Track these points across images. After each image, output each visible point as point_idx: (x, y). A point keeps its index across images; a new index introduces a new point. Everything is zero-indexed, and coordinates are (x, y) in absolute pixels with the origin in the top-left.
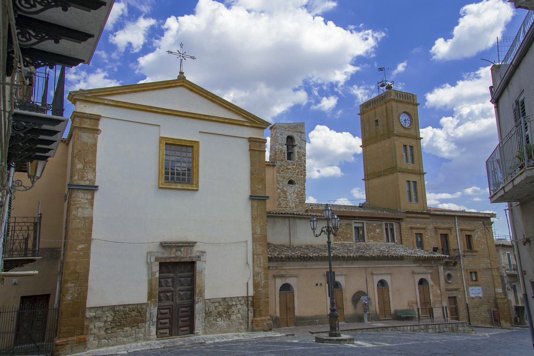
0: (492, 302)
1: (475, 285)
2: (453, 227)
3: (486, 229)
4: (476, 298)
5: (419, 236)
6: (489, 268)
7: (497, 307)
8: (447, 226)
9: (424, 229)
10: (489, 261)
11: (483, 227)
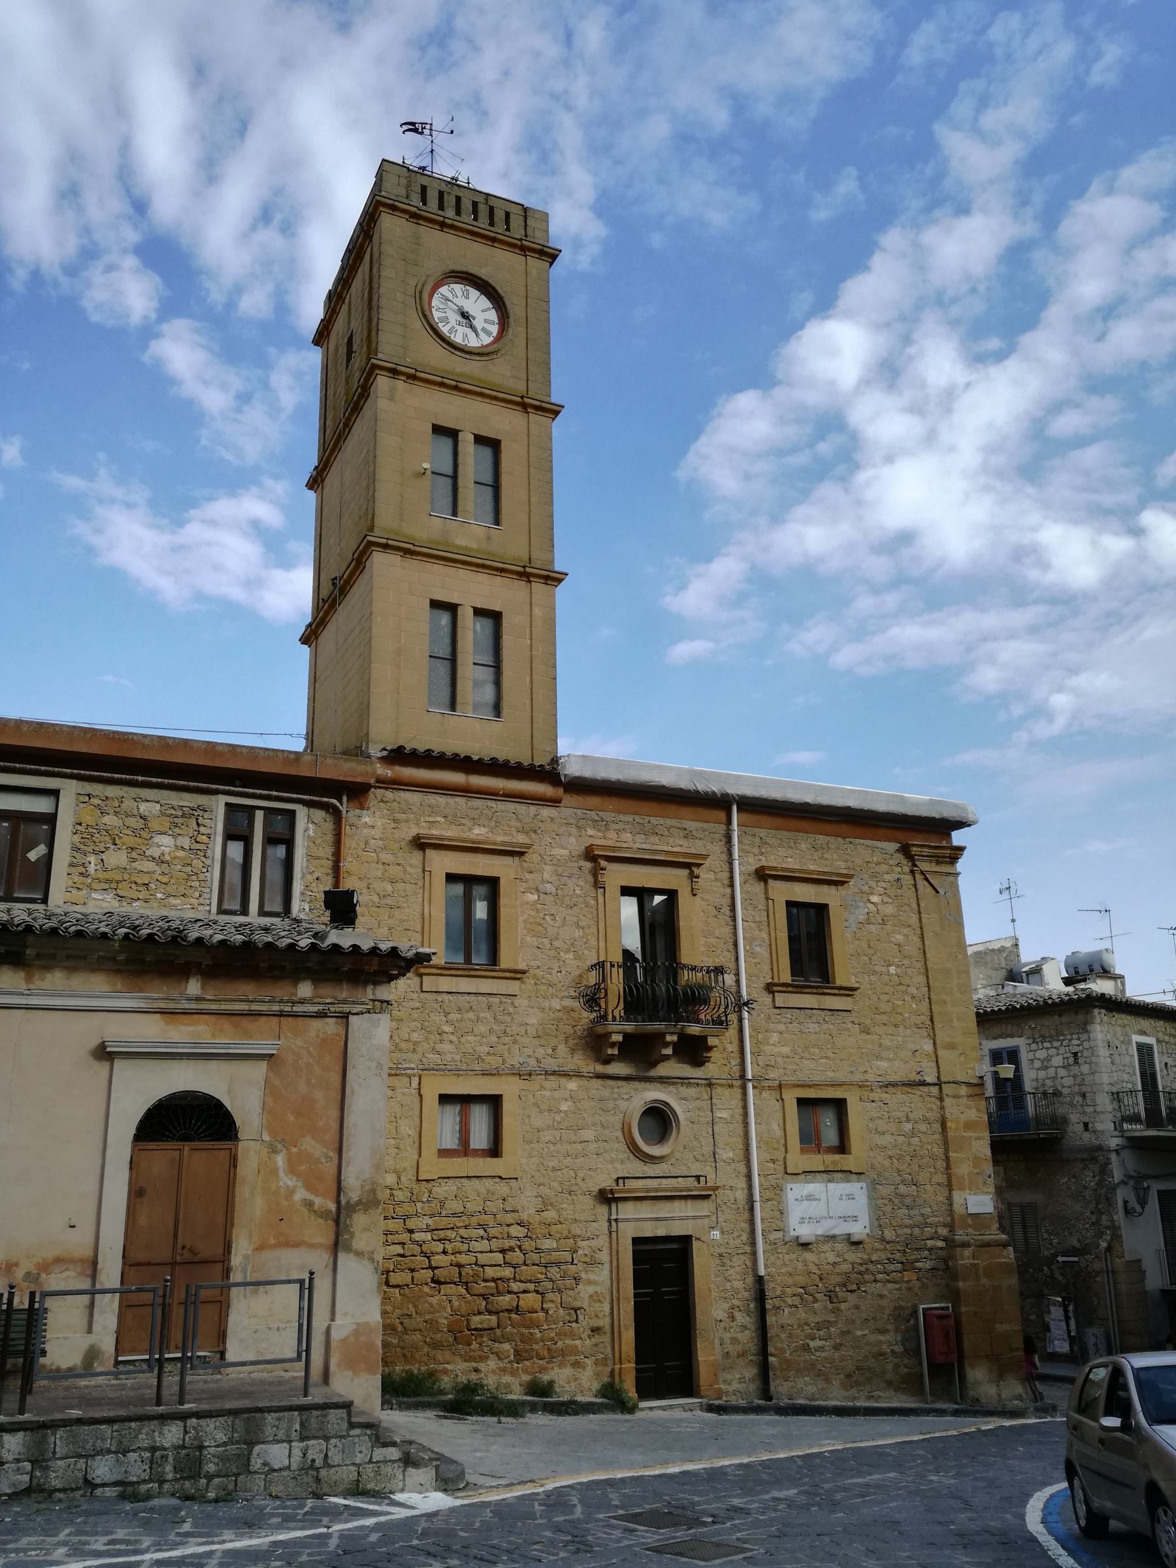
0: (928, 1265)
1: (829, 1173)
2: (706, 857)
3: (921, 883)
4: (826, 1247)
5: (480, 890)
6: (923, 1083)
7: (954, 1296)
8: (676, 845)
9: (517, 853)
10: (928, 1046)
11: (907, 869)
